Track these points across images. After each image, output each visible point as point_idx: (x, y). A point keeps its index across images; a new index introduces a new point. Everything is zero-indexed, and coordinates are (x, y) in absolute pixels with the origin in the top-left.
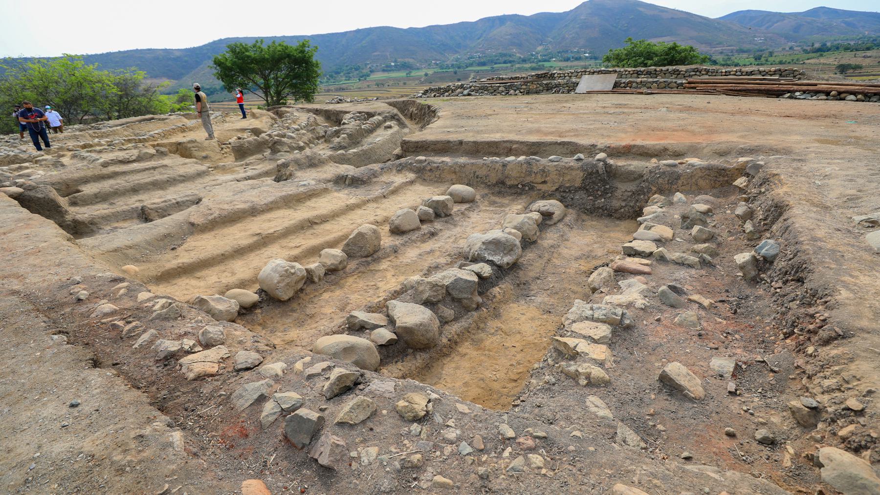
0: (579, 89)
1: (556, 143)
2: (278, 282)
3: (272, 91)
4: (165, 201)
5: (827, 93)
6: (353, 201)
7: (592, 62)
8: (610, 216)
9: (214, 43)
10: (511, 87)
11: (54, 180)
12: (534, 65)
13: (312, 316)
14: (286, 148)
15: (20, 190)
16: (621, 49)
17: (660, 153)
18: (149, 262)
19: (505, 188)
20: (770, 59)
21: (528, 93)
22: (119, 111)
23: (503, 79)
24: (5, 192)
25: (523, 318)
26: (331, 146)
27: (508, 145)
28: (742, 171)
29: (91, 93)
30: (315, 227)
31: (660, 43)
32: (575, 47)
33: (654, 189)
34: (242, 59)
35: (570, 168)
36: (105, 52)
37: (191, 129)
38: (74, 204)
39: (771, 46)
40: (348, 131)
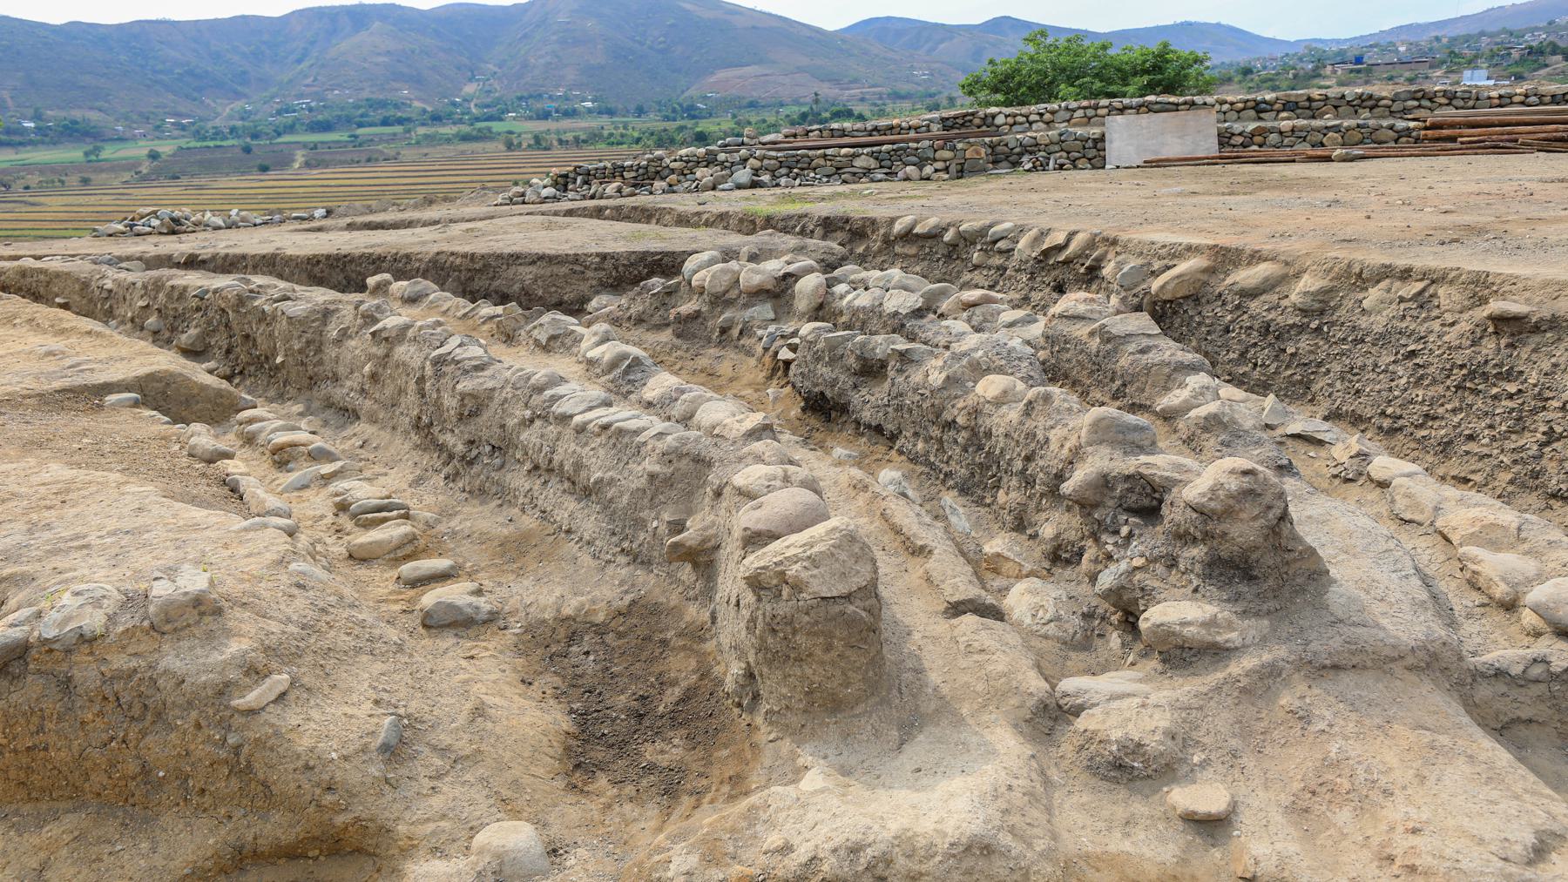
7: (604, 120)
12: (465, 129)
16: (983, 70)
32: (557, 87)
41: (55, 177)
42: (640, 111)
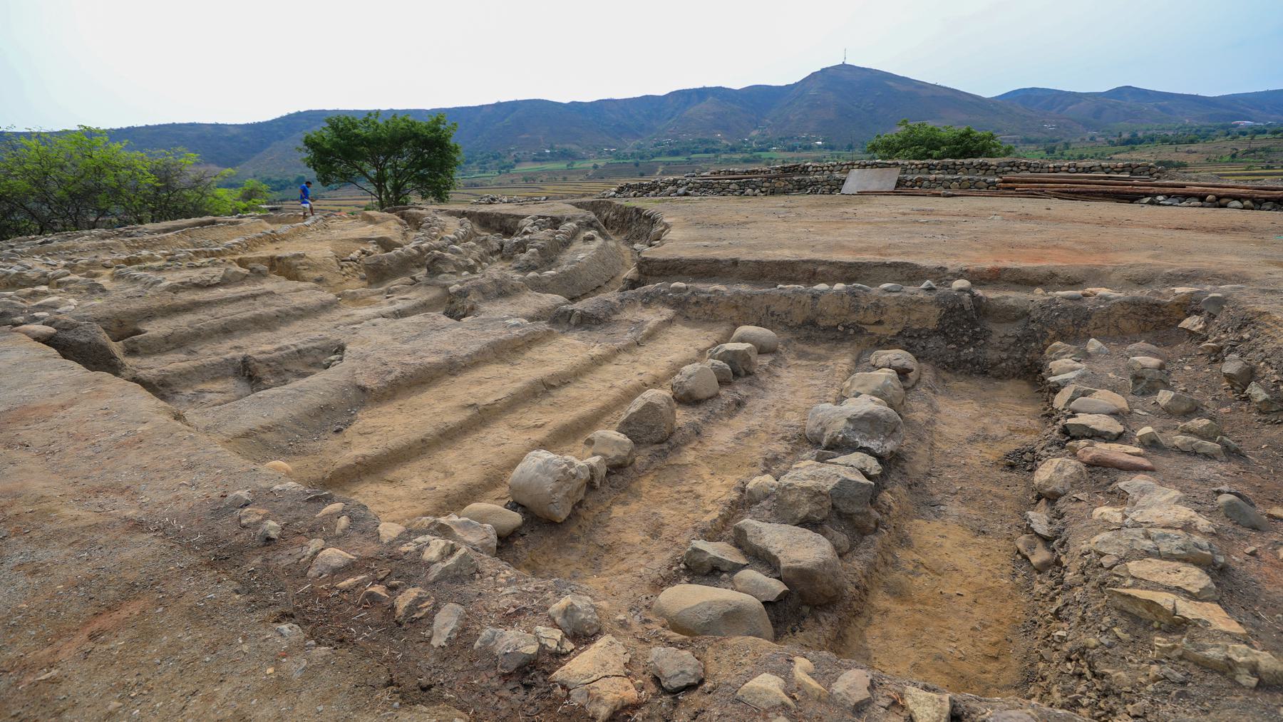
0: (846, 188)
1: (884, 265)
2: (554, 492)
3: (388, 184)
4: (280, 349)
5: (1202, 198)
6: (596, 351)
7: (827, 153)
8: (984, 373)
9: (289, 116)
10: (747, 184)
11: (100, 313)
12: (747, 156)
13: (609, 549)
14: (451, 268)
15: (51, 330)
16: (896, 132)
17: (1047, 280)
18: (304, 454)
19: (818, 331)
20: (1066, 152)
21: (773, 193)
22: (153, 211)
23: (734, 173)
24: (27, 333)
25: (948, 544)
26: (516, 265)
27: (810, 267)
28: (1188, 307)
29: (115, 184)
30: (554, 393)
31: (948, 126)
33: (1052, 333)
34: (348, 138)
35: (920, 302)
36: (124, 126)
37: (284, 238)
38: (132, 352)
39: (1066, 135)
40: (538, 244)
41: (553, 177)
42: (850, 147)
